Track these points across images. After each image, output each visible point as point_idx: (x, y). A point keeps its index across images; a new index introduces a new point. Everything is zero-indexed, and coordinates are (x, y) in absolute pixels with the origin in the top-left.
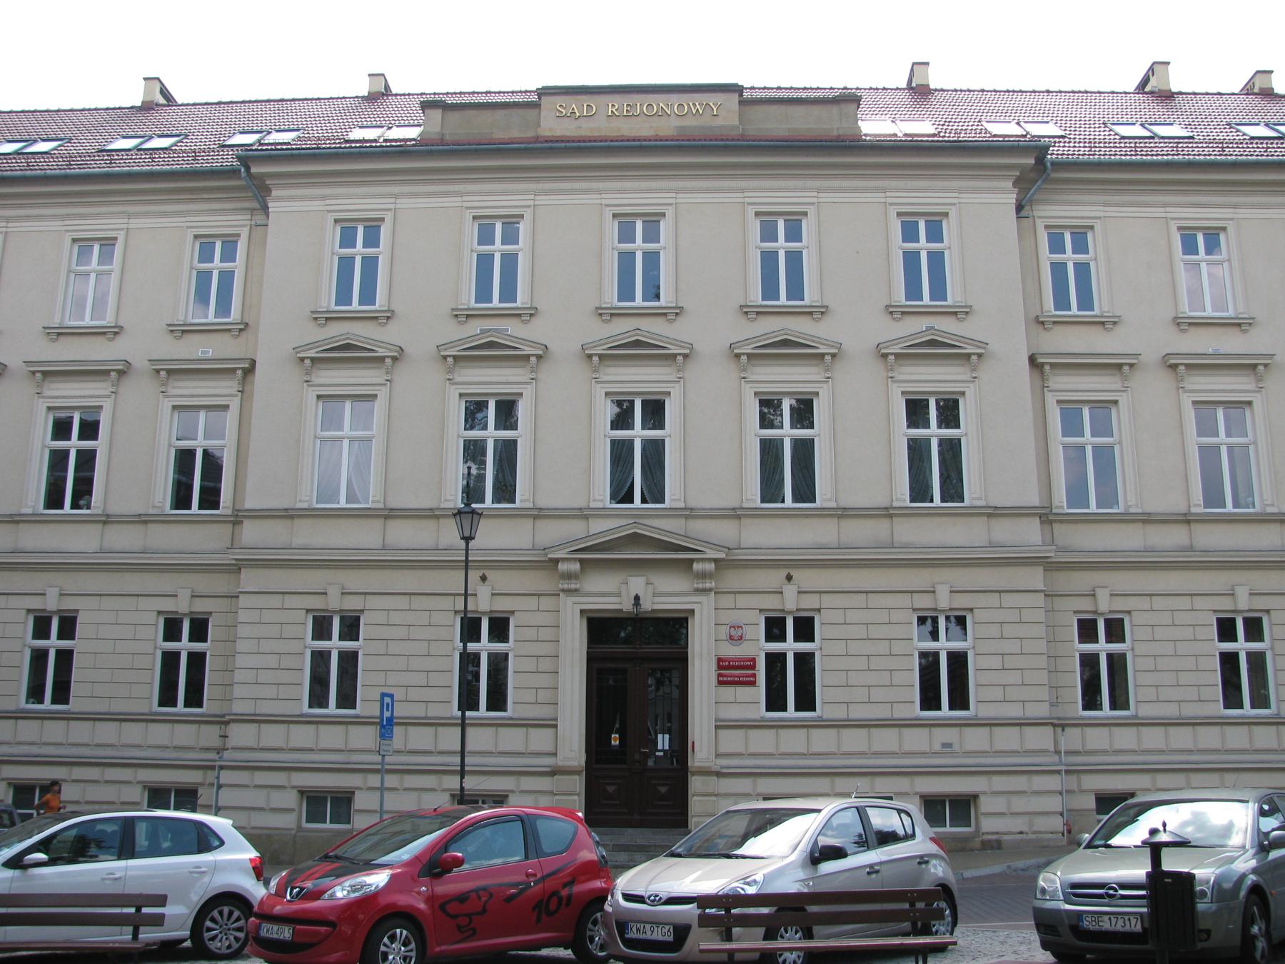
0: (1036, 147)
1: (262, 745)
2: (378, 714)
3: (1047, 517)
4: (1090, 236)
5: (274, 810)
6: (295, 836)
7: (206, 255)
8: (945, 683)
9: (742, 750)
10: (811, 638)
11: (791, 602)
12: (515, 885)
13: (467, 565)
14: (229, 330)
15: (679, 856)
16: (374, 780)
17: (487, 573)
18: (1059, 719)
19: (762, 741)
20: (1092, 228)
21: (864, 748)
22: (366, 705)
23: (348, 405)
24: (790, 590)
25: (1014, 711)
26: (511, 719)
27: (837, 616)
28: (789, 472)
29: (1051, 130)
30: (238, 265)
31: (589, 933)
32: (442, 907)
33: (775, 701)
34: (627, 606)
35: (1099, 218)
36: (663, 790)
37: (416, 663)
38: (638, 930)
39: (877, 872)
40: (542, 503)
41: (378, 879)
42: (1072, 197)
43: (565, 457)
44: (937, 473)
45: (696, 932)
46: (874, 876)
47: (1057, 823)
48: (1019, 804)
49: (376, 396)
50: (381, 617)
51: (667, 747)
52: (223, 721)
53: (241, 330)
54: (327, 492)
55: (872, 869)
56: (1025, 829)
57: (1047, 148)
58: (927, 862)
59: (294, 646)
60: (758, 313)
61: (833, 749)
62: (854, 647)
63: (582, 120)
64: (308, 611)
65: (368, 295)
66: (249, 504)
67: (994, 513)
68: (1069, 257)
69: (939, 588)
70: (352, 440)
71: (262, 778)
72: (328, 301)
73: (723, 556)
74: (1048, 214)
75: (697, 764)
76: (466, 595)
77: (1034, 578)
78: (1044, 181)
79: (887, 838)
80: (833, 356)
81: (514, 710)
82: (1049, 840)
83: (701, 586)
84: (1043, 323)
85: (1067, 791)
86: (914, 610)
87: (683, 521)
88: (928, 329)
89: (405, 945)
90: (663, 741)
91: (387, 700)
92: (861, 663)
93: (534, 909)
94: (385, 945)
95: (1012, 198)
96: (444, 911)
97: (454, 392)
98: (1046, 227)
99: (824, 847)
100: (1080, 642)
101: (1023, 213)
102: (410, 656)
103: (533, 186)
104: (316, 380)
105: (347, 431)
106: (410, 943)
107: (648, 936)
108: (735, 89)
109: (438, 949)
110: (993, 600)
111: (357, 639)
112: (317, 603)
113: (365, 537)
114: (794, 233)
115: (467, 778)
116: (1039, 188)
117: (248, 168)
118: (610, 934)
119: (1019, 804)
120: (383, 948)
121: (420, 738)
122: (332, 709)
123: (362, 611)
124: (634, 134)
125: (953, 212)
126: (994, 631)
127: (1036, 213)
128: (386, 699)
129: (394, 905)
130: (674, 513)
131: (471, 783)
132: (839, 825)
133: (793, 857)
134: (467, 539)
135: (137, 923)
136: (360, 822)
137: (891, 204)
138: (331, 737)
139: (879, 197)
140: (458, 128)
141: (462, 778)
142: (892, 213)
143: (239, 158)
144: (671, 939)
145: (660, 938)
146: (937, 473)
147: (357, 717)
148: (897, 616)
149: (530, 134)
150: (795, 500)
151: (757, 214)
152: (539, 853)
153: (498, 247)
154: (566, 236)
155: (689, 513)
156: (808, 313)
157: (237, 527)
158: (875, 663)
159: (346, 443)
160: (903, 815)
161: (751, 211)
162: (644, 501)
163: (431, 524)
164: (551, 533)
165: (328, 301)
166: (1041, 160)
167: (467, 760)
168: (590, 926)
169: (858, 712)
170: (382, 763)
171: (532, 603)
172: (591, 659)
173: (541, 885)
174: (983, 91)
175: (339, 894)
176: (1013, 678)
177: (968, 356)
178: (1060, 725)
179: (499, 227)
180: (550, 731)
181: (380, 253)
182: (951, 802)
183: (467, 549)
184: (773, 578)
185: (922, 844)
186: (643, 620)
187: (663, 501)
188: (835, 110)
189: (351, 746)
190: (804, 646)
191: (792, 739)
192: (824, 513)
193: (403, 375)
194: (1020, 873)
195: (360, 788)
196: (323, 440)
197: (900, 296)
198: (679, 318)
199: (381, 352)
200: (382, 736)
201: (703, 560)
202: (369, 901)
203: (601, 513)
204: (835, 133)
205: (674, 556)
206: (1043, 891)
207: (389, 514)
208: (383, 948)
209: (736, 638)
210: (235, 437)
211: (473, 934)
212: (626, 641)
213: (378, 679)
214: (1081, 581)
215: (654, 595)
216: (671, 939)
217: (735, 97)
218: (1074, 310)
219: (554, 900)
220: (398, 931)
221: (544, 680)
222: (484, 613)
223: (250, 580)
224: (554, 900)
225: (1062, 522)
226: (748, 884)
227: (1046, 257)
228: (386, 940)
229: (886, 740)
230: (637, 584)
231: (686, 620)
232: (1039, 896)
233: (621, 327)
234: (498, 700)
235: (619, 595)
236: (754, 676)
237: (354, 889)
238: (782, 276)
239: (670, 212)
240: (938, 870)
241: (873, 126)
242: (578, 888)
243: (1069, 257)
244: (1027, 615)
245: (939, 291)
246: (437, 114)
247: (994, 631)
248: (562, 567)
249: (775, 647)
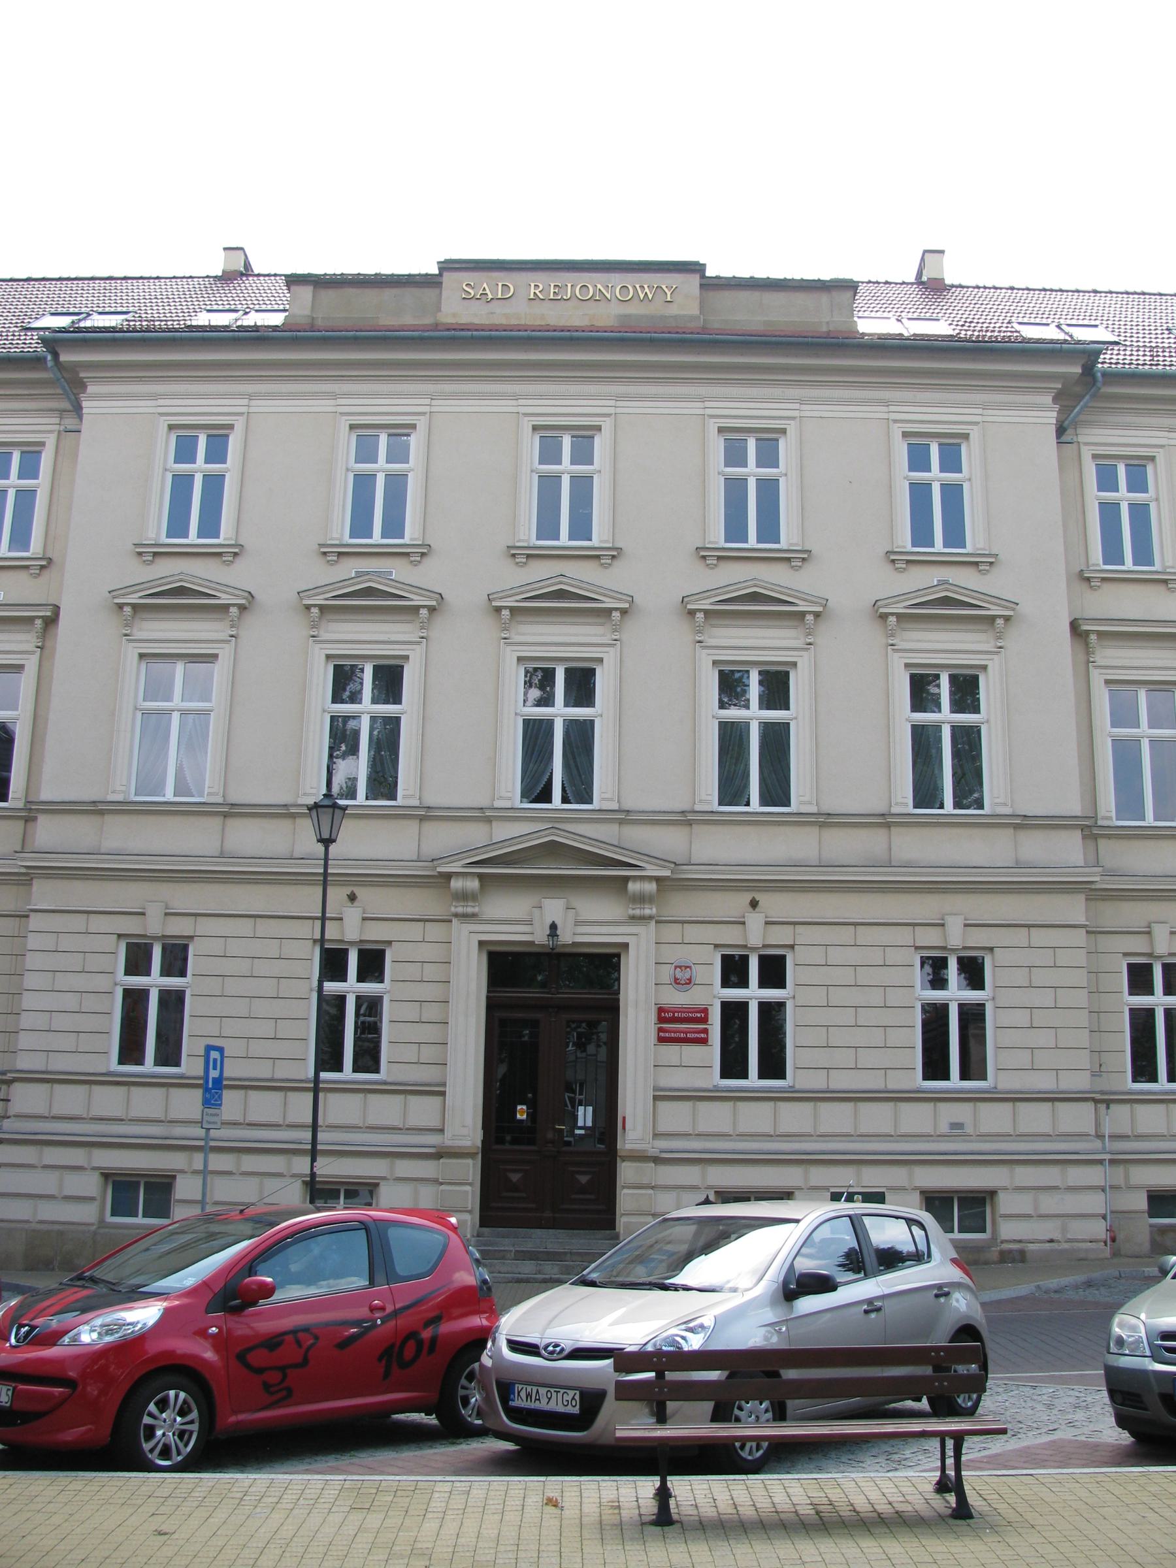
0: (1084, 352)
1: (56, 1111)
2: (201, 1073)
3: (1091, 830)
4: (1150, 469)
5: (68, 1198)
6: (95, 1233)
7: (366, 452)
8: (950, 1044)
10: (781, 984)
11: (756, 936)
12: (357, 1323)
13: (325, 880)
14: (27, 567)
15: (592, 1284)
16: (198, 1160)
17: (359, 891)
18: (1102, 1093)
19: (715, 1117)
20: (1152, 459)
21: (848, 1129)
22: (190, 1065)
23: (180, 667)
24: (755, 921)
25: (1043, 1082)
26: (385, 1083)
27: (817, 956)
28: (756, 767)
29: (1101, 334)
30: (42, 483)
31: (461, 1392)
32: (241, 1357)
33: (733, 1065)
34: (539, 936)
35: (1162, 446)
36: (584, 1179)
37: (262, 1008)
38: (529, 1395)
39: (878, 1310)
40: (431, 800)
41: (144, 1315)
42: (1129, 419)
43: (463, 737)
44: (948, 769)
45: (610, 1406)
46: (873, 1315)
47: (1099, 1229)
48: (1050, 1204)
49: (216, 656)
50: (216, 946)
51: (589, 1123)
53: (42, 567)
54: (150, 779)
55: (872, 1306)
56: (1056, 1235)
57: (1098, 353)
58: (947, 1294)
59: (101, 982)
60: (719, 558)
61: (808, 1129)
62: (837, 996)
63: (495, 302)
64: (120, 936)
65: (210, 525)
66: (46, 794)
67: (1023, 823)
68: (1123, 496)
69: (949, 920)
70: (184, 713)
71: (54, 1156)
72: (157, 531)
73: (667, 873)
75: (628, 1146)
76: (323, 919)
77: (1074, 909)
78: (1093, 396)
79: (890, 1259)
80: (817, 615)
81: (389, 1072)
82: (1087, 1250)
83: (637, 912)
84: (1088, 579)
85: (1111, 1187)
86: (917, 948)
87: (615, 827)
88: (942, 583)
89: (182, 1413)
90: (585, 1116)
92: (847, 1017)
93: (380, 1359)
94: (151, 1415)
95: (1051, 417)
96: (248, 1366)
97: (318, 655)
98: (1095, 457)
99: (803, 1276)
100: (1131, 994)
101: (1064, 439)
102: (252, 997)
103: (430, 387)
104: (138, 634)
105: (177, 702)
106: (190, 1411)
107: (543, 1405)
108: (695, 268)
109: (233, 1419)
110: (1020, 937)
111: (382, 981)
112: (131, 926)
113: (196, 840)
114: (768, 457)
115: (321, 1161)
116: (1086, 406)
117: (56, 355)
118: (488, 1399)
119: (1050, 1204)
120: (147, 1420)
121: (264, 1106)
122: (149, 1065)
123: (191, 937)
124: (562, 323)
125: (975, 434)
126: (1020, 977)
127: (1081, 439)
128: (213, 1053)
129: (171, 1353)
131: (328, 1168)
132: (823, 1240)
133: (759, 1290)
134: (327, 842)
136: (179, 1213)
137: (895, 421)
138: (147, 1102)
139: (880, 412)
140: (335, 310)
141: (313, 1160)
142: (897, 431)
143: (44, 341)
144: (576, 1410)
145: (561, 1409)
146: (948, 769)
147: (182, 1077)
148: (894, 956)
149: (428, 321)
150: (764, 801)
151: (721, 430)
152: (391, 1276)
154: (472, 453)
155: (624, 817)
156: (594, 557)
157: (30, 824)
158: (865, 1017)
159: (176, 716)
160: (915, 1229)
161: (713, 426)
162: (565, 800)
163: (286, 824)
164: (443, 839)
165: (157, 531)
166: (1089, 369)
167: (321, 1136)
168: (463, 1381)
169: (841, 1081)
170: (207, 1138)
171: (414, 931)
172: (492, 1006)
173: (392, 1323)
174: (1012, 288)
175: (86, 1338)
176: (1044, 1038)
177: (993, 619)
178: (1104, 1101)
179: (383, 439)
180: (436, 1101)
181: (227, 470)
182: (959, 1199)
183: (326, 859)
184: (733, 904)
185: (941, 1268)
186: (560, 956)
187: (590, 802)
188: (824, 298)
189: (173, 1115)
191: (754, 1116)
192: (803, 820)
193: (253, 629)
194: (1052, 1295)
195: (182, 1171)
196: (146, 713)
197: (904, 539)
198: (616, 563)
199: (225, 599)
200: (207, 1103)
202: (130, 1347)
203: (509, 815)
204: (824, 329)
205: (605, 873)
206: (1120, 1342)
207: (230, 811)
208: (147, 1420)
209: (683, 983)
210: (30, 706)
211: (288, 1396)
212: (543, 985)
213: (211, 1027)
214: (1133, 914)
215: (578, 923)
216: (576, 1410)
217: (695, 279)
218: (1129, 564)
219: (411, 1346)
220: (172, 1393)
221: (429, 1033)
222: (352, 943)
223: (44, 894)
224: (411, 1346)
225: (1109, 837)
226: (691, 1330)
227: (1094, 496)
228: (152, 1407)
229: (876, 1118)
230: (554, 909)
231: (618, 956)
232: (1113, 1349)
233: (540, 573)
234: (368, 1058)
235: (530, 923)
236: (706, 1031)
237: (108, 1330)
238: (752, 512)
239: (607, 425)
240: (962, 1304)
241: (869, 325)
242: (447, 1327)
243: (1123, 496)
244: (1064, 958)
245: (955, 535)
246: (306, 292)
247: (1020, 977)
248: (456, 884)
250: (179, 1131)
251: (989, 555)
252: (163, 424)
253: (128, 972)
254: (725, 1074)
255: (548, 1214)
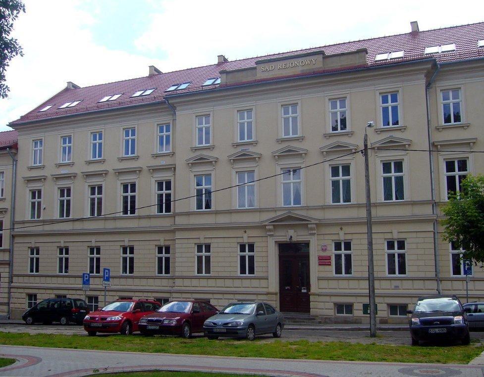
9: (241, 286)
10: (169, 253)
11: (342, 237)
16: (103, 293)
25: (422, 275)
33: (338, 271)
52: (173, 278)
53: (172, 155)
73: (318, 222)
74: (444, 85)
77: (430, 227)
84: (438, 129)
91: (106, 271)
95: (422, 82)
110: (414, 235)
111: (404, 249)
112: (197, 241)
122: (204, 274)
130: (302, 208)
135: (162, 336)
137: (279, 102)
140: (231, 80)
147: (211, 276)
153: (390, 104)
155: (308, 208)
156: (347, 134)
170: (467, 295)
171: (260, 239)
184: (336, 230)
188: (357, 56)
190: (348, 252)
200: (84, 283)
201: (311, 224)
215: (297, 236)
223: (178, 235)
230: (291, 232)
235: (286, 236)
246: (224, 76)
249: (338, 252)
250: (187, 288)
251: (405, 126)
252: (279, 105)
253: (158, 254)
254: (241, 273)
255: (296, 309)
